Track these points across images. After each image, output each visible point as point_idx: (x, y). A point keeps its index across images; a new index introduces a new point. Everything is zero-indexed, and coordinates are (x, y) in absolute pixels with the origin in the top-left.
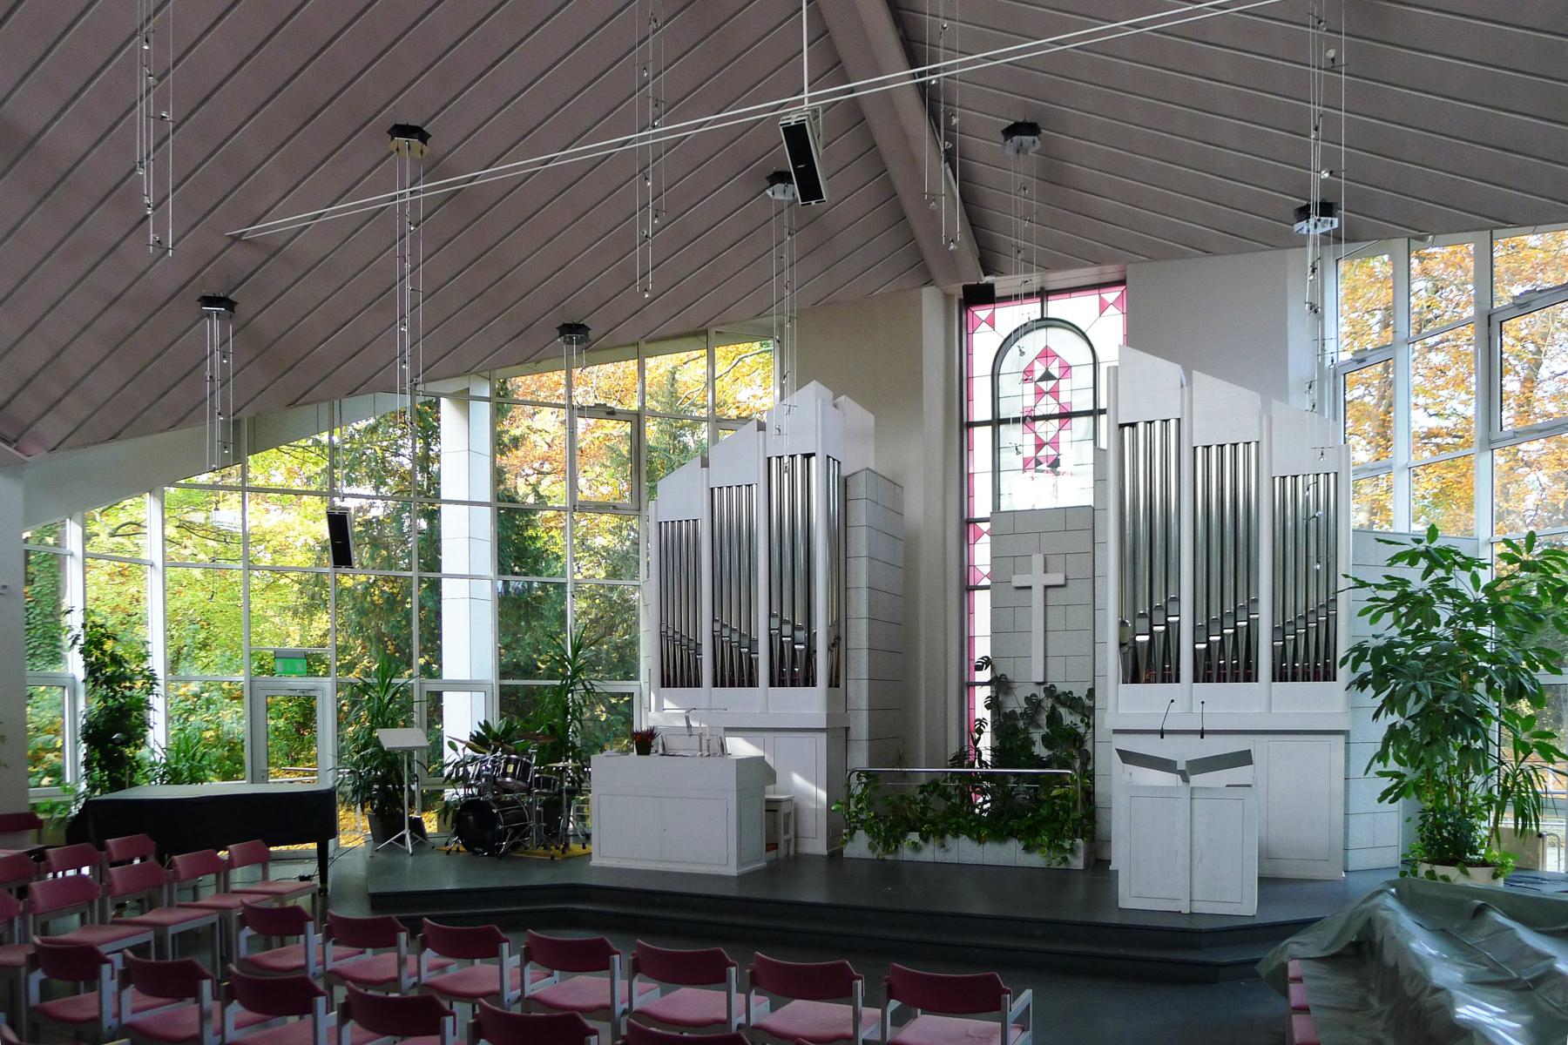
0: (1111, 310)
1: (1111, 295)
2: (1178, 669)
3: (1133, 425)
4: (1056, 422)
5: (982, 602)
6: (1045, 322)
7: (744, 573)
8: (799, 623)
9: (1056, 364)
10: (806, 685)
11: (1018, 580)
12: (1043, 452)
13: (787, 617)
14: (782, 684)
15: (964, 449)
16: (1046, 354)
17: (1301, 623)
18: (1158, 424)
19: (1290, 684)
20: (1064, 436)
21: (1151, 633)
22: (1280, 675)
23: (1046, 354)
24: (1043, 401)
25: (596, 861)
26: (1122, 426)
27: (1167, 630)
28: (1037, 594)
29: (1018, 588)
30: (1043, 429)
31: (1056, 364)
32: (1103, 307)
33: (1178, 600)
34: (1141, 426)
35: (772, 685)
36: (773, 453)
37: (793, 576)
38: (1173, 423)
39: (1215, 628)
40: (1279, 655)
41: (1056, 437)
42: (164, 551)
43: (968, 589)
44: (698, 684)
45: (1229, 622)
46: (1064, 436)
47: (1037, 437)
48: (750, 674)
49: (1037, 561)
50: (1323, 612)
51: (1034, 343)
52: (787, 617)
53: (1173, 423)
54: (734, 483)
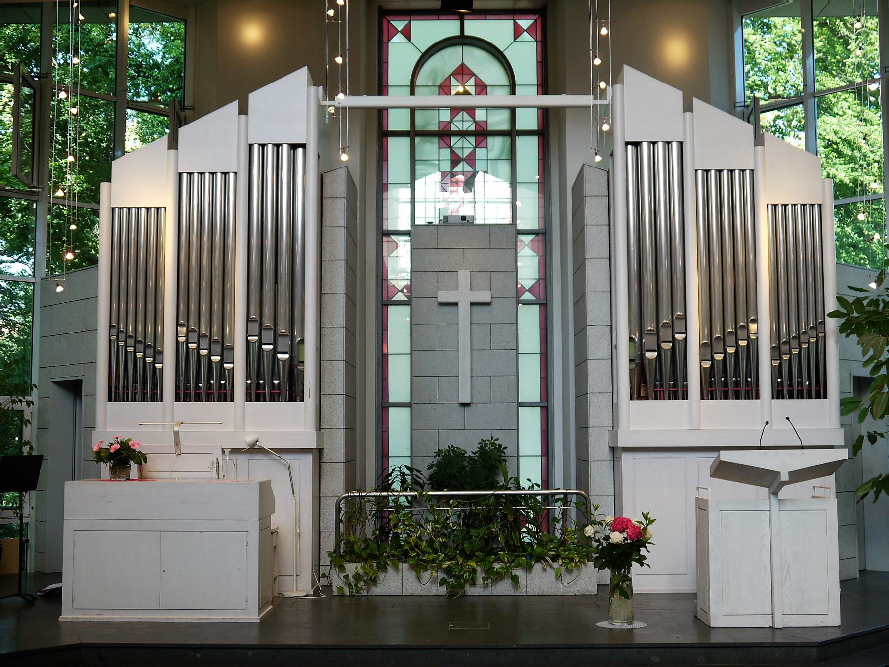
0: (525, 36)
1: (525, 23)
2: (757, 385)
3: (637, 145)
4: (472, 140)
5: (399, 321)
6: (462, 40)
7: (217, 271)
8: (203, 332)
9: (472, 81)
10: (291, 399)
11: (444, 296)
12: (459, 168)
13: (267, 323)
14: (187, 398)
15: (382, 157)
16: (463, 72)
17: (794, 343)
18: (660, 144)
19: (731, 403)
20: (480, 153)
21: (659, 349)
22: (708, 393)
23: (463, 72)
24: (459, 117)
25: (67, 615)
26: (627, 144)
27: (673, 348)
28: (464, 309)
29: (442, 304)
30: (459, 145)
31: (472, 81)
32: (517, 32)
33: (684, 317)
34: (645, 145)
35: (177, 399)
36: (255, 139)
37: (276, 276)
38: (675, 146)
39: (718, 347)
40: (707, 377)
41: (473, 154)
42: (449, 78)
43: (385, 303)
44: (685, 396)
45: (731, 340)
46: (480, 153)
47: (453, 153)
48: (154, 384)
49: (464, 276)
50: (813, 333)
51: (450, 59)
52: (267, 323)
53: (675, 146)
54: (207, 169)
